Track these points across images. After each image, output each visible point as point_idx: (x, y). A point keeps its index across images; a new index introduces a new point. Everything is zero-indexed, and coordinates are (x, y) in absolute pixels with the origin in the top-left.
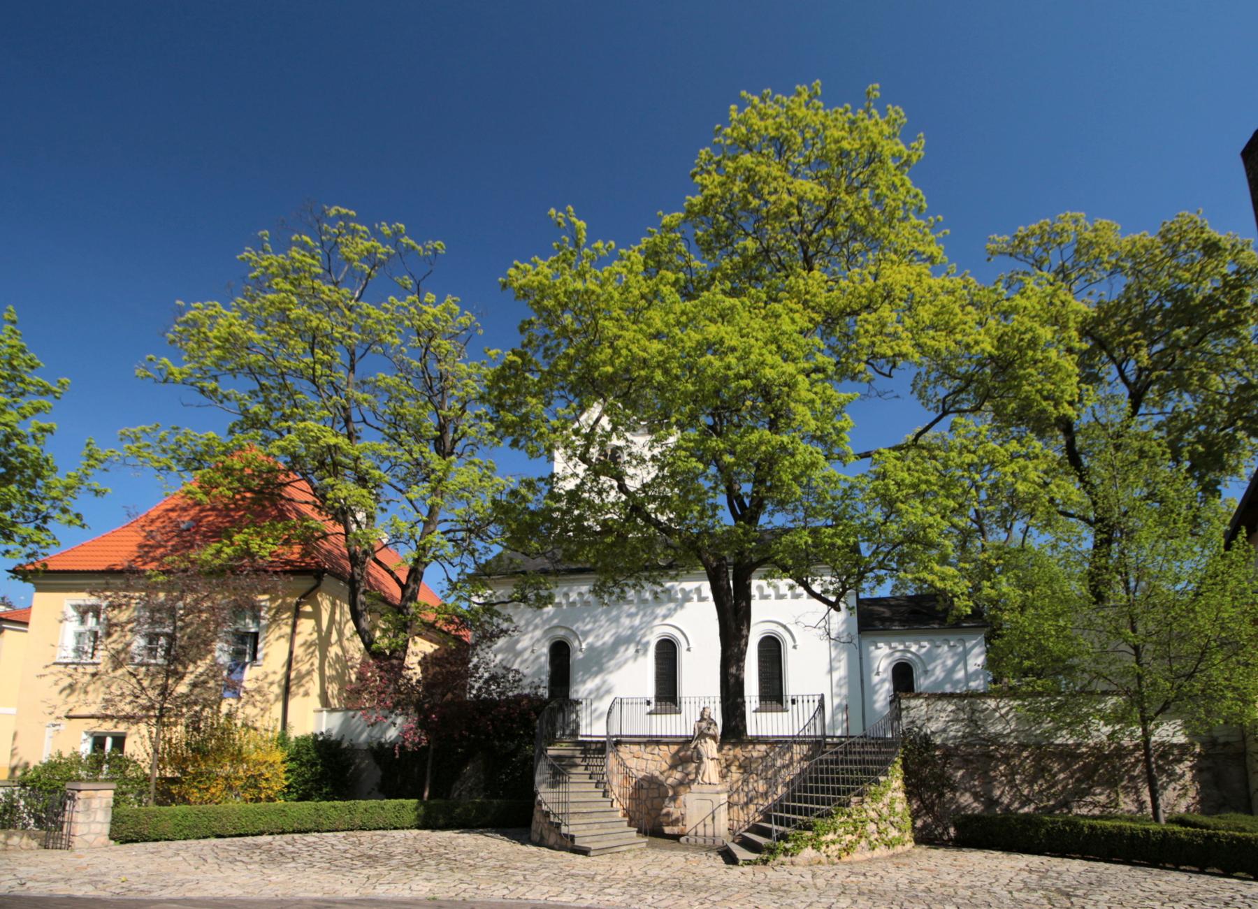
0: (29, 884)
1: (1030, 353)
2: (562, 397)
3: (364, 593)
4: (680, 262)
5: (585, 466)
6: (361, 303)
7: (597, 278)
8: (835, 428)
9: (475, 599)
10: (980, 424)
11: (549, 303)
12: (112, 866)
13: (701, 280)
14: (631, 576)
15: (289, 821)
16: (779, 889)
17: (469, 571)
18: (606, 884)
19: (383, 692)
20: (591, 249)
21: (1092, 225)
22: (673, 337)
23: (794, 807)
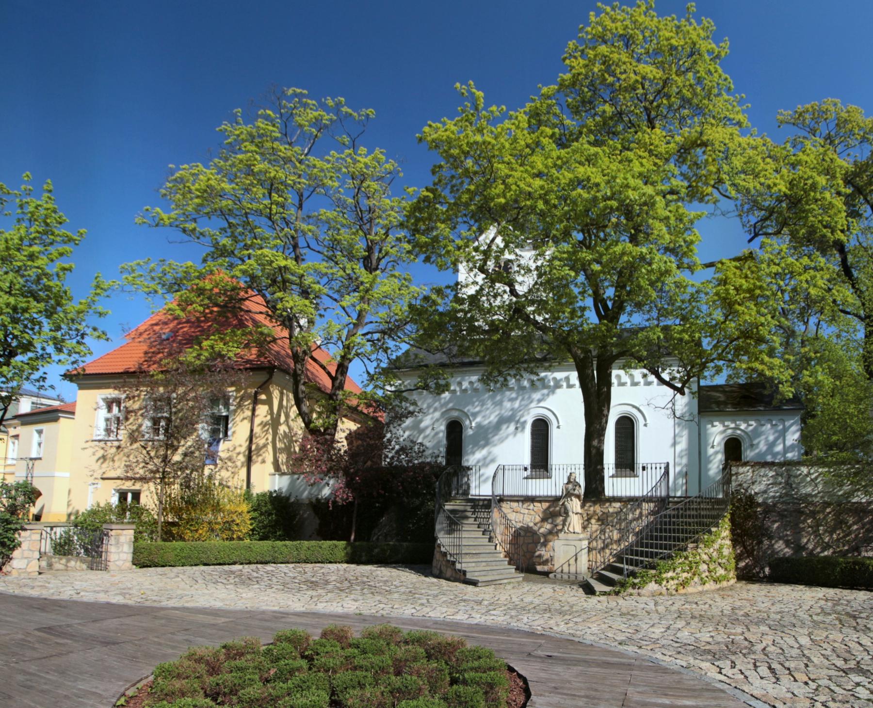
0: (82, 594)
1: (812, 194)
2: (465, 222)
3: (304, 383)
4: (555, 121)
5: (484, 276)
6: (309, 157)
7: (492, 132)
8: (685, 241)
9: (388, 388)
10: (781, 244)
11: (455, 152)
12: (135, 583)
13: (571, 134)
14: (513, 367)
15: (254, 555)
16: (628, 614)
17: (384, 365)
18: (491, 608)
19: (320, 460)
20: (487, 111)
21: (845, 107)
22: (551, 176)
23: (642, 552)
